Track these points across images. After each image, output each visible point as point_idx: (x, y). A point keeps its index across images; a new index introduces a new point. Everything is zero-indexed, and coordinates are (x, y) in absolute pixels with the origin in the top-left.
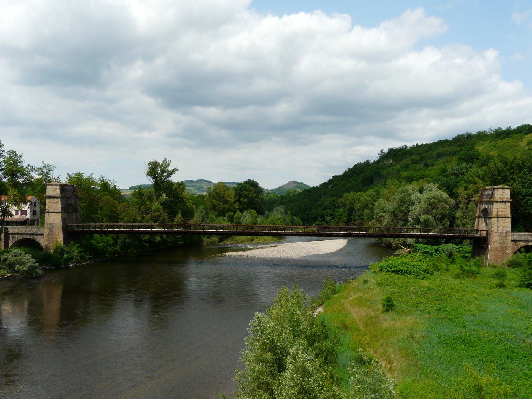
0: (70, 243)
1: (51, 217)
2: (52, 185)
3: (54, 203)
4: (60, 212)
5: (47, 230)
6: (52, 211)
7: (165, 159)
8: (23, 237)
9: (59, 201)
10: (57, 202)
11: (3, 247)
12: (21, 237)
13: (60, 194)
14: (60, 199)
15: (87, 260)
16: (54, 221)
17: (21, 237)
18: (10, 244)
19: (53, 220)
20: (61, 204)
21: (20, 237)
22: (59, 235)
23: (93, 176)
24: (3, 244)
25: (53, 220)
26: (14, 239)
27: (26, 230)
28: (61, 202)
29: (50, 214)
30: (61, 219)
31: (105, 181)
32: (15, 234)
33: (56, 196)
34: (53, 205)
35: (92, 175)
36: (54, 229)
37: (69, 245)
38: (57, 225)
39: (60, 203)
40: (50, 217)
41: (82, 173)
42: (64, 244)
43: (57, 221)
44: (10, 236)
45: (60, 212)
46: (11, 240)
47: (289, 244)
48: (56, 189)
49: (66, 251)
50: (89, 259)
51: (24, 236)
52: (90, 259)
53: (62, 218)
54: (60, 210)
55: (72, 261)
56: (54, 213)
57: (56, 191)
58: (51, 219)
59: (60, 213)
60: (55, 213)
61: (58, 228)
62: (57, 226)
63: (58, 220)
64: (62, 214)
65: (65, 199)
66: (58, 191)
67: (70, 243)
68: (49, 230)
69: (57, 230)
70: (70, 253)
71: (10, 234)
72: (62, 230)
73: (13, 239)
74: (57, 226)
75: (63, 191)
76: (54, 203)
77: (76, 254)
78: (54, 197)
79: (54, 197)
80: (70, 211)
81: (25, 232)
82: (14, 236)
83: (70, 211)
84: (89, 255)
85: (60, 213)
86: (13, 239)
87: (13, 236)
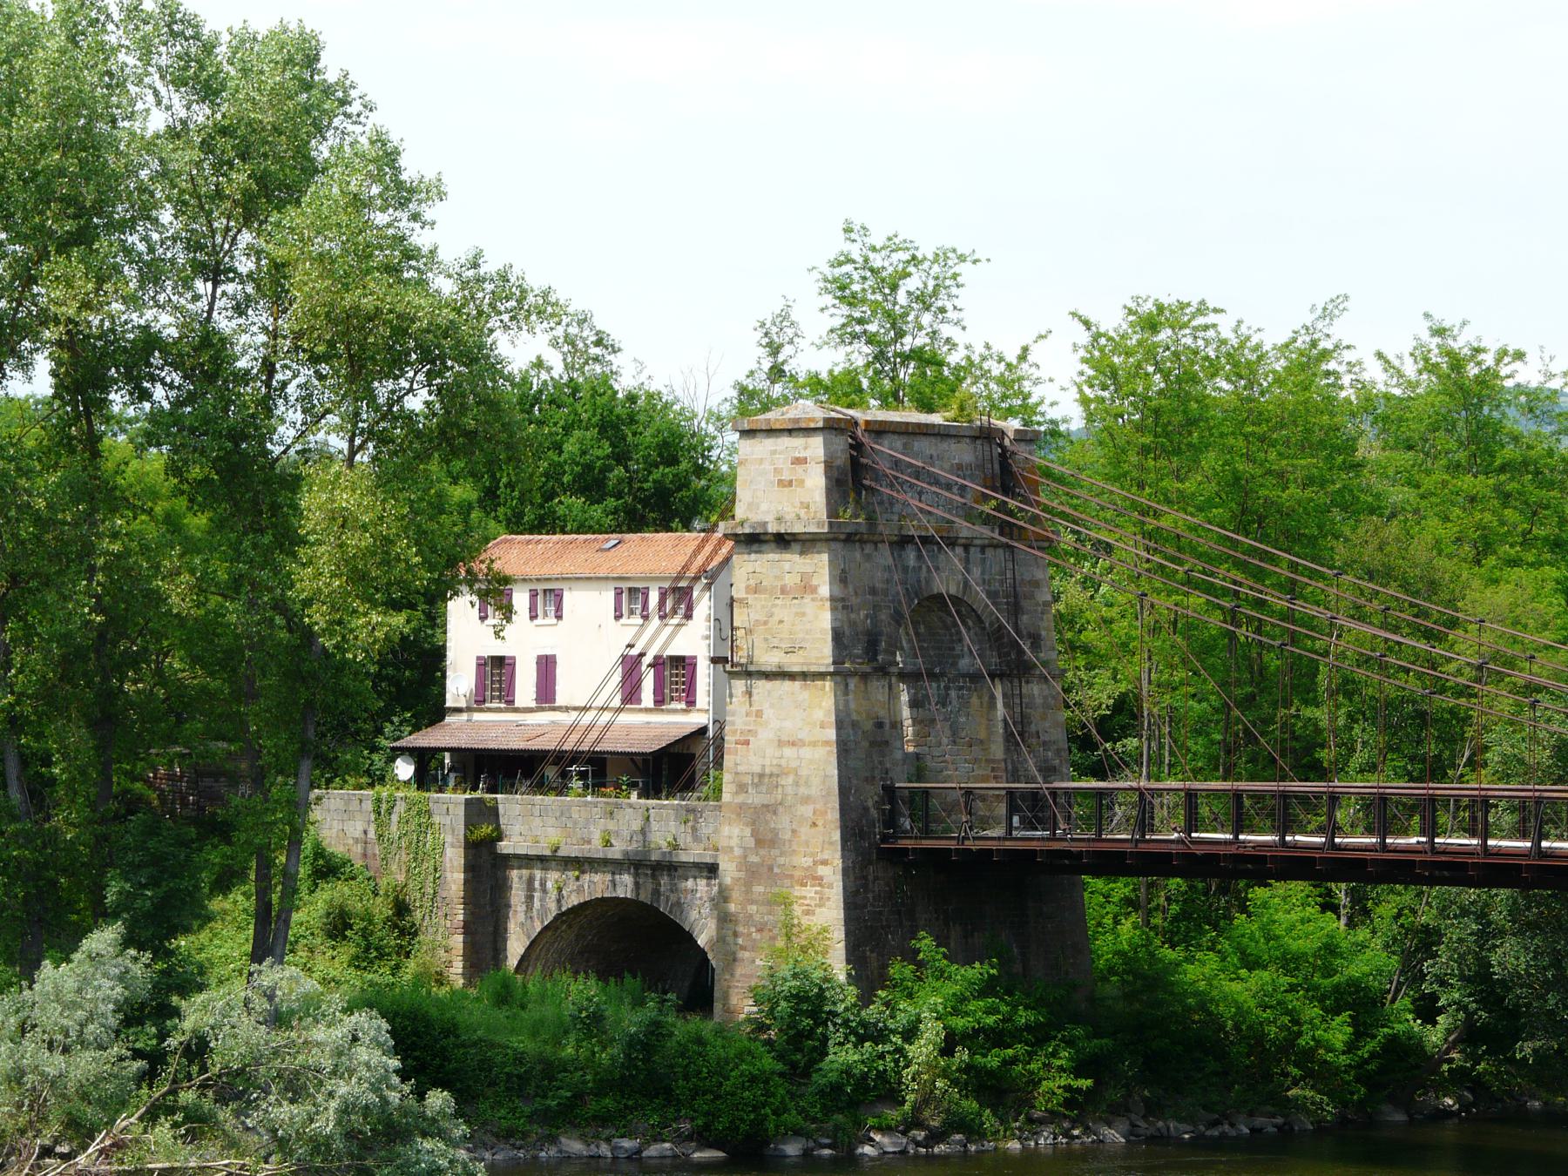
0: (911, 956)
1: (768, 713)
2: (771, 432)
3: (783, 591)
4: (821, 676)
5: (736, 831)
6: (768, 659)
7: (619, 350)
8: (596, 885)
9: (818, 568)
10: (807, 588)
11: (458, 966)
12: (580, 890)
13: (832, 513)
14: (825, 557)
15: (1052, 1117)
16: (788, 752)
17: (580, 890)
18: (516, 947)
19: (781, 744)
20: (839, 604)
21: (572, 885)
22: (819, 880)
23: (1340, 331)
24: (460, 938)
25: (781, 744)
26: (537, 904)
27: (611, 826)
28: (841, 577)
29: (761, 686)
30: (831, 734)
31: (1472, 371)
32: (542, 861)
33: (798, 528)
34: (780, 613)
35: (1327, 314)
36: (783, 823)
37: (899, 970)
38: (803, 791)
39: (825, 590)
40: (759, 714)
41: (1202, 309)
42: (854, 954)
43: (806, 752)
44: (514, 874)
45: (821, 676)
46: (521, 908)
47: (634, 750)
48: (799, 469)
49: (846, 1022)
50: (1068, 1104)
51: (597, 878)
52: (1077, 1107)
53: (840, 725)
54: (821, 654)
55: (893, 1115)
56: (787, 685)
57: (801, 482)
58: (765, 736)
59: (828, 684)
60: (791, 676)
61: (806, 811)
62: (806, 800)
63: (814, 744)
64: (843, 690)
65: (885, 549)
66: (815, 482)
67: (911, 956)
68: (748, 832)
69: (805, 831)
70: (879, 1036)
71: (507, 857)
72: (836, 836)
73: (530, 898)
74: (806, 800)
75: (858, 486)
76: (783, 591)
77: (922, 1050)
78: (783, 541)
79: (783, 541)
80: (964, 663)
81: (608, 844)
82: (538, 874)
83: (964, 663)
84: (1078, 1073)
85: (828, 684)
86: (530, 898)
87: (531, 880)
